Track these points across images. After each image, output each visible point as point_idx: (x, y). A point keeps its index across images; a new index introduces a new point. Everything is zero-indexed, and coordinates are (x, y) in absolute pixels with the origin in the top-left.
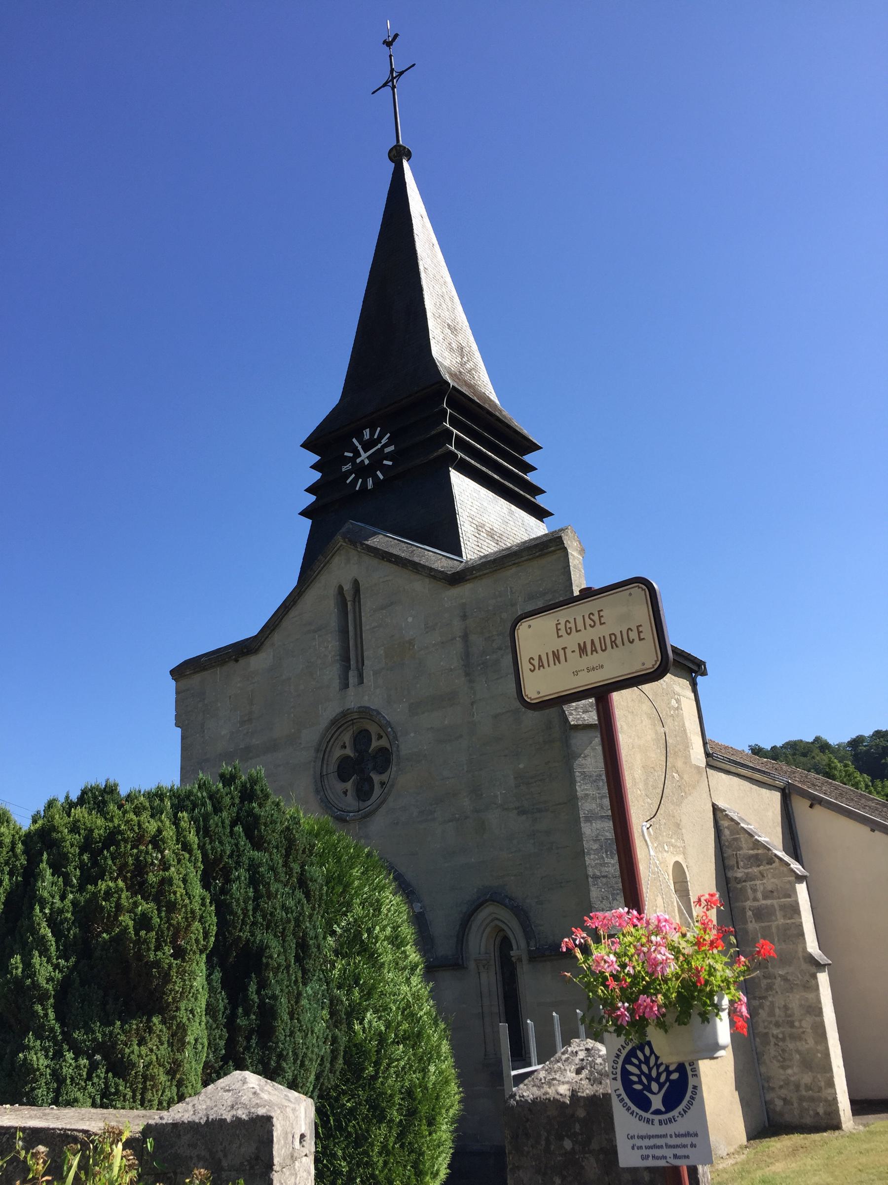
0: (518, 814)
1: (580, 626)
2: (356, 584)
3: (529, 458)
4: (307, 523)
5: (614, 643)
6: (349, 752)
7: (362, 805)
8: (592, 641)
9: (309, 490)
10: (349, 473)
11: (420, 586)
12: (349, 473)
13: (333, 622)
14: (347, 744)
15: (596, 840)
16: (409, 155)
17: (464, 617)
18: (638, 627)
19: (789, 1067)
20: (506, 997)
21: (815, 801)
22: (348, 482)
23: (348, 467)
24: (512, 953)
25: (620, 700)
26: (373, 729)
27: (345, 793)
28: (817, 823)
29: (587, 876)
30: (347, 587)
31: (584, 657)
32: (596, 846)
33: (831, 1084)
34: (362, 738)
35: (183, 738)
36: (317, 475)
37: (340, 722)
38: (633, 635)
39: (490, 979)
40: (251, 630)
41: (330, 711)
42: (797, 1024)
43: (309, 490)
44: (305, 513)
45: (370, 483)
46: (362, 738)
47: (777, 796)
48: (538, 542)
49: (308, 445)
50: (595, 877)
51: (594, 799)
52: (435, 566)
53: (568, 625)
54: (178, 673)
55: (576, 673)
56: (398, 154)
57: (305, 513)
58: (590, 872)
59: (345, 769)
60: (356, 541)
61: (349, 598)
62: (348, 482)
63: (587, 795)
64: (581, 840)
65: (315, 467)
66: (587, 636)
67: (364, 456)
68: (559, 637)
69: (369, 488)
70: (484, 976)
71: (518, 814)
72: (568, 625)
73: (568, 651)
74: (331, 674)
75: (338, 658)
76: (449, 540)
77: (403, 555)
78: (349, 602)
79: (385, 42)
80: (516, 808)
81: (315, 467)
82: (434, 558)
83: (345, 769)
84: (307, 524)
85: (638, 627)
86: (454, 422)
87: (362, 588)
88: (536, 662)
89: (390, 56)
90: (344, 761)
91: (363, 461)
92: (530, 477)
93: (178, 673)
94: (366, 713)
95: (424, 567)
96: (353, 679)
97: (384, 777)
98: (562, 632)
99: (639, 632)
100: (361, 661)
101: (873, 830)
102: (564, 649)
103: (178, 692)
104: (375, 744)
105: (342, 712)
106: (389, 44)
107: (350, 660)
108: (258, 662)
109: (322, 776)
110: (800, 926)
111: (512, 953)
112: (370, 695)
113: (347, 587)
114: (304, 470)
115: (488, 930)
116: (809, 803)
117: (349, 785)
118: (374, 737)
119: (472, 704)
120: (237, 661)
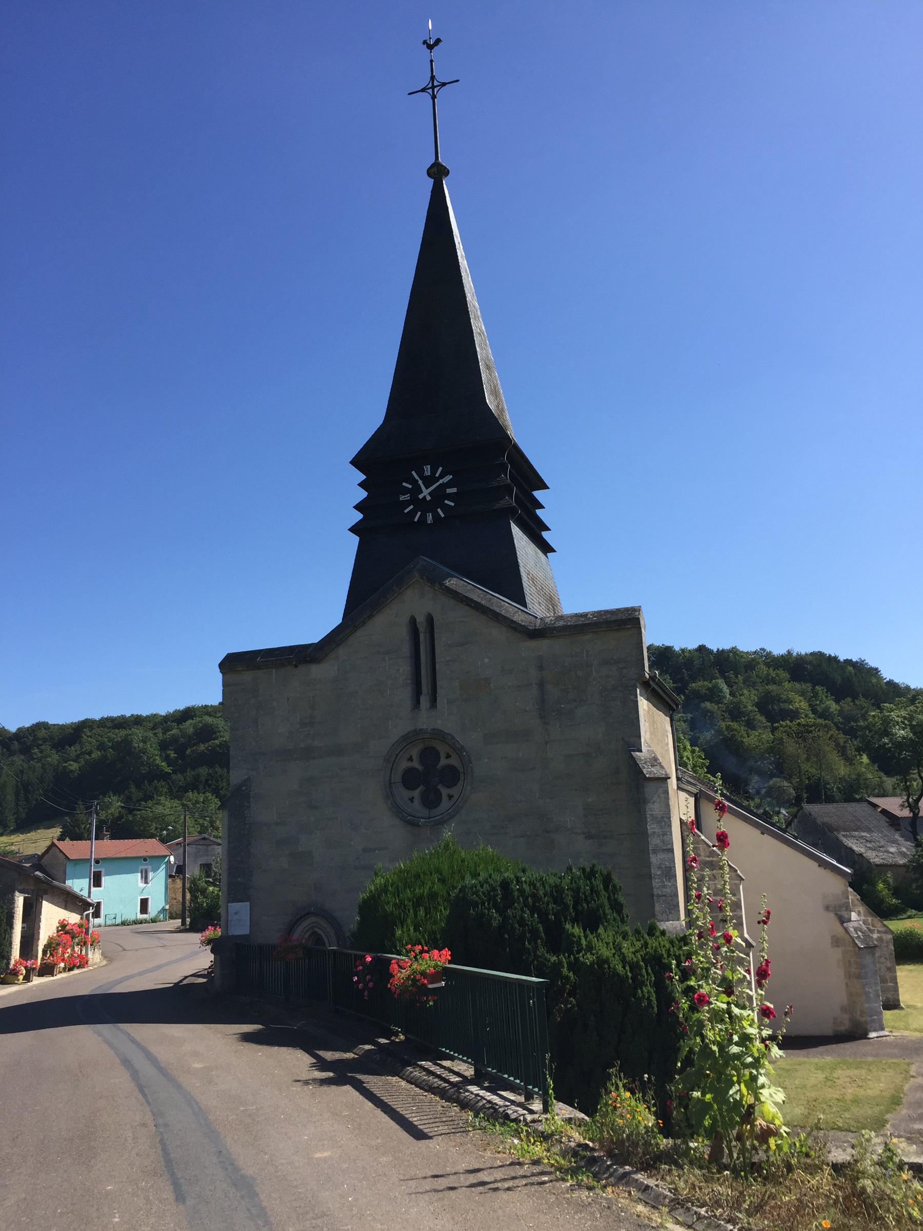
0: (586, 838)
2: (430, 620)
6: (416, 764)
10: (408, 503)
11: (497, 632)
12: (408, 503)
13: (406, 649)
14: (414, 758)
15: (660, 868)
16: (446, 172)
17: (541, 668)
22: (406, 511)
23: (407, 497)
26: (442, 749)
27: (412, 800)
29: (653, 895)
30: (421, 620)
32: (659, 873)
34: (429, 755)
36: (363, 494)
37: (409, 739)
41: (399, 728)
43: (358, 507)
44: (354, 530)
45: (430, 518)
46: (429, 755)
47: (692, 800)
48: (614, 618)
50: (659, 896)
51: (659, 836)
52: (515, 619)
56: (438, 172)
57: (354, 530)
58: (656, 892)
59: (410, 779)
60: (434, 580)
61: (422, 628)
62: (406, 511)
63: (654, 833)
64: (649, 867)
65: (362, 485)
67: (426, 493)
69: (429, 522)
71: (586, 838)
74: (404, 694)
75: (409, 681)
77: (483, 602)
78: (421, 635)
79: (425, 42)
80: (584, 833)
81: (362, 485)
82: (505, 605)
83: (410, 779)
84: (355, 540)
89: (432, 61)
90: (409, 772)
91: (425, 497)
94: (439, 735)
95: (505, 618)
96: (425, 701)
103: (225, 685)
104: (443, 762)
105: (415, 730)
106: (430, 47)
108: (317, 671)
109: (390, 783)
112: (444, 718)
113: (421, 620)
114: (351, 488)
117: (416, 793)
118: (443, 756)
119: (546, 743)
120: (296, 666)
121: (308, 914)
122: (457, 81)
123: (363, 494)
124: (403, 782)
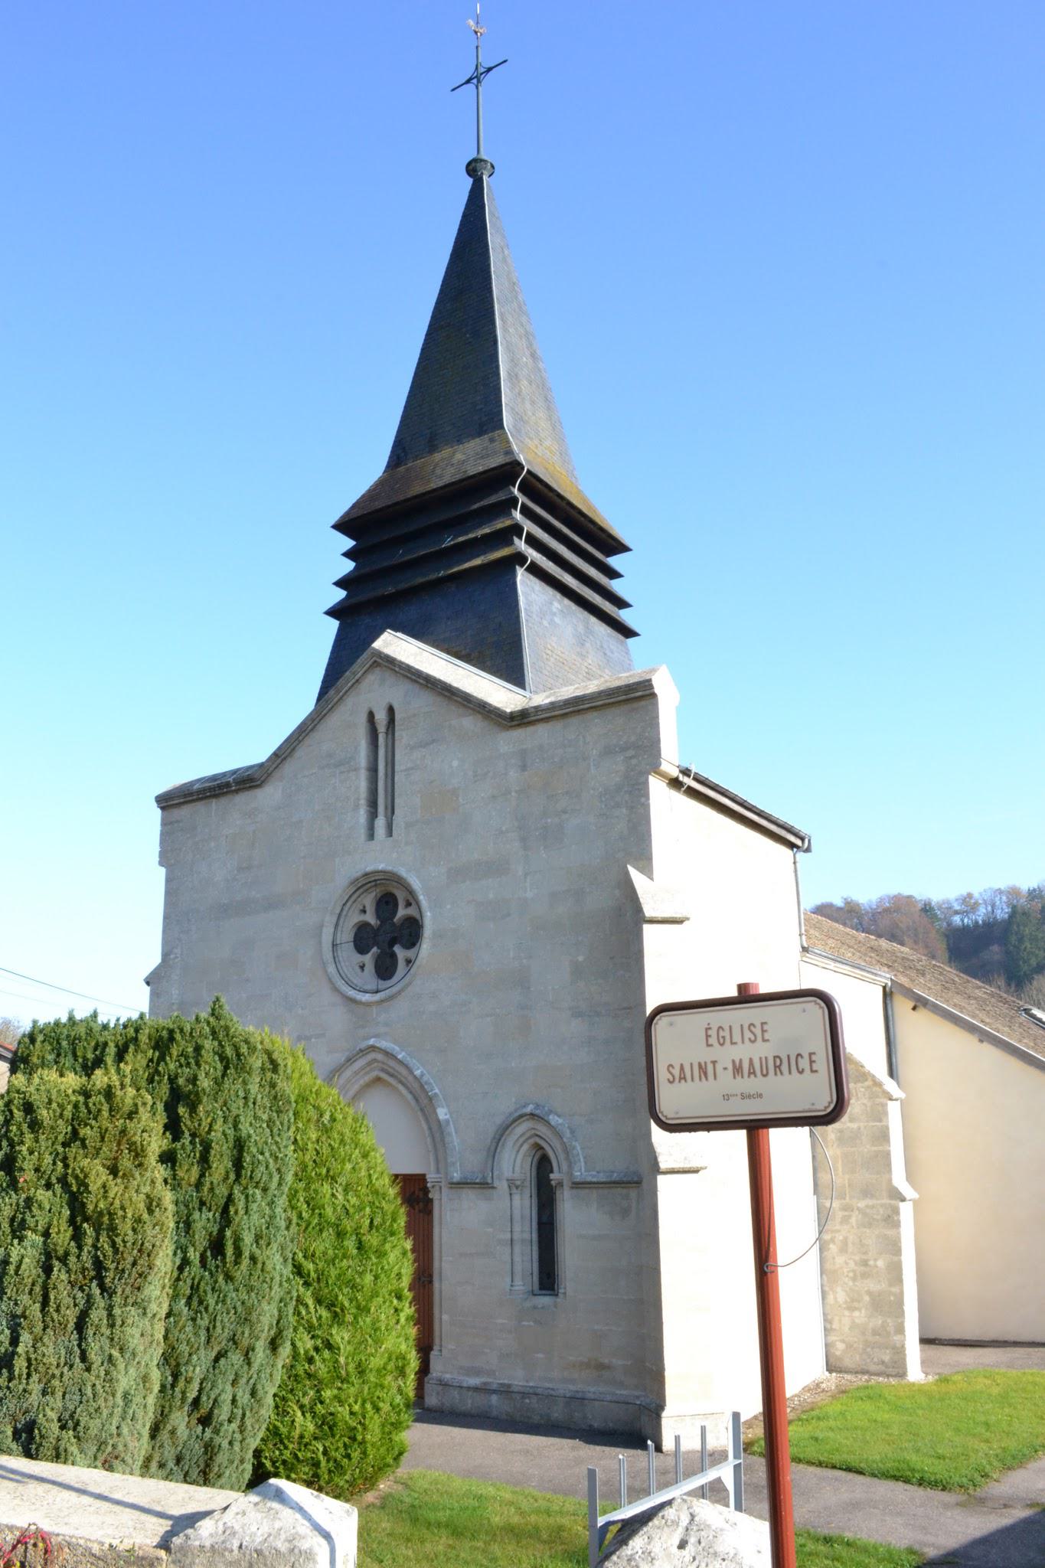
1: (737, 1038)
3: (614, 561)
4: (334, 624)
5: (778, 1068)
6: (371, 918)
7: (383, 984)
8: (751, 1060)
9: (339, 584)
14: (368, 909)
18: (810, 1054)
19: (856, 1309)
20: (540, 1224)
21: (920, 1003)
24: (552, 1176)
25: (777, 1137)
27: (362, 967)
28: (915, 1026)
31: (739, 1078)
33: (900, 1330)
35: (168, 881)
36: (349, 566)
38: (804, 1063)
39: (524, 1204)
40: (257, 753)
42: (871, 1263)
43: (339, 584)
44: (332, 613)
46: (387, 903)
49: (343, 526)
53: (721, 1033)
54: (168, 801)
55: (727, 1097)
57: (332, 613)
61: (381, 729)
65: (348, 554)
66: (743, 1052)
68: (708, 1045)
70: (517, 1198)
72: (721, 1033)
73: (719, 1068)
76: (507, 663)
81: (348, 554)
85: (810, 1054)
86: (526, 512)
87: (398, 717)
88: (676, 1072)
92: (615, 586)
93: (168, 801)
96: (380, 822)
97: (410, 953)
98: (713, 1040)
99: (812, 1062)
100: (391, 810)
101: (981, 1041)
102: (714, 1063)
103: (164, 823)
107: (379, 801)
108: (269, 795)
110: (887, 1155)
111: (552, 1176)
115: (526, 1147)
116: (912, 1004)
121: (521, 1116)
122: (696, 1171)
123: (349, 566)
124: (355, 941)
